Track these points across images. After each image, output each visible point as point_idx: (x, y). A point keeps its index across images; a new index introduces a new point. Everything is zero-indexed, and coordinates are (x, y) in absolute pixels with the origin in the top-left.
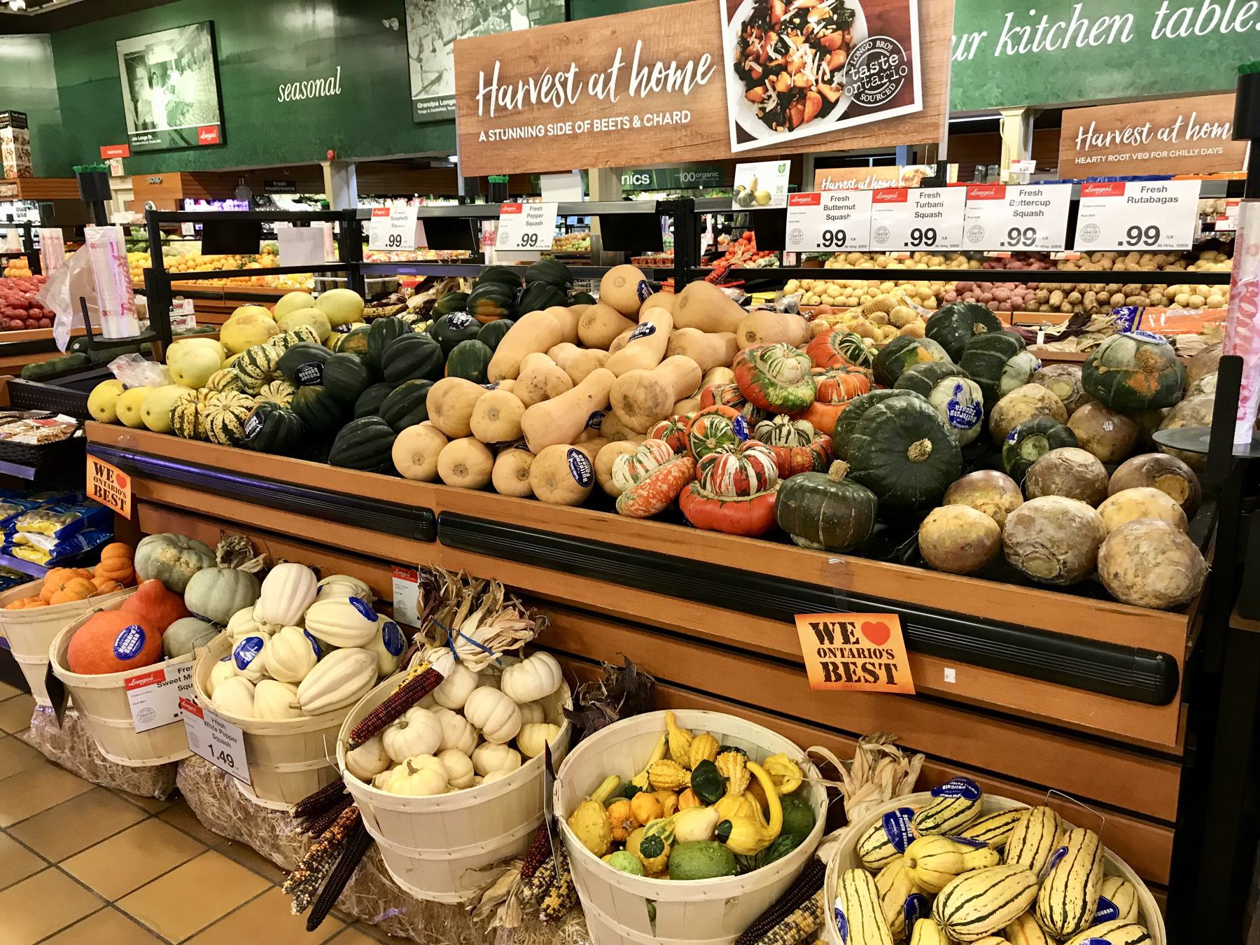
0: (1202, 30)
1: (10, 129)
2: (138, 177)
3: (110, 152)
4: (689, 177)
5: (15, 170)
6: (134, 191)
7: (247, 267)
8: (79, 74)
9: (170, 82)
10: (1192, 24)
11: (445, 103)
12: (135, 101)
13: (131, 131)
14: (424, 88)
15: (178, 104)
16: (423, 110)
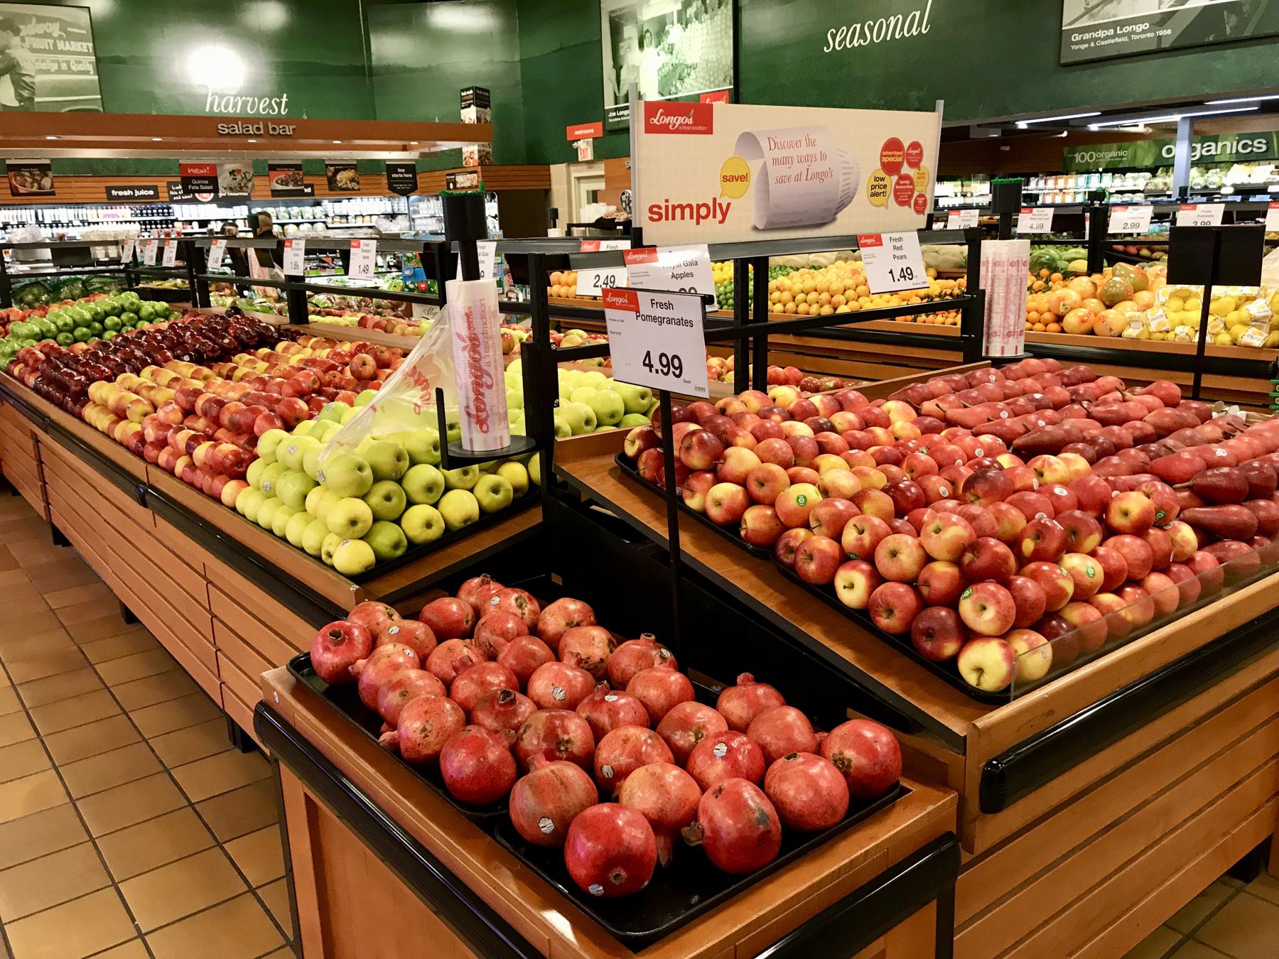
0: (878, 38)
1: (473, 108)
2: (614, 162)
3: (577, 133)
4: (1087, 157)
5: (476, 157)
6: (606, 178)
7: (909, 317)
8: (546, 42)
9: (669, 40)
10: (920, 25)
11: (1128, 29)
12: (618, 67)
13: (609, 104)
14: (1088, 11)
15: (675, 67)
16: (1079, 45)
